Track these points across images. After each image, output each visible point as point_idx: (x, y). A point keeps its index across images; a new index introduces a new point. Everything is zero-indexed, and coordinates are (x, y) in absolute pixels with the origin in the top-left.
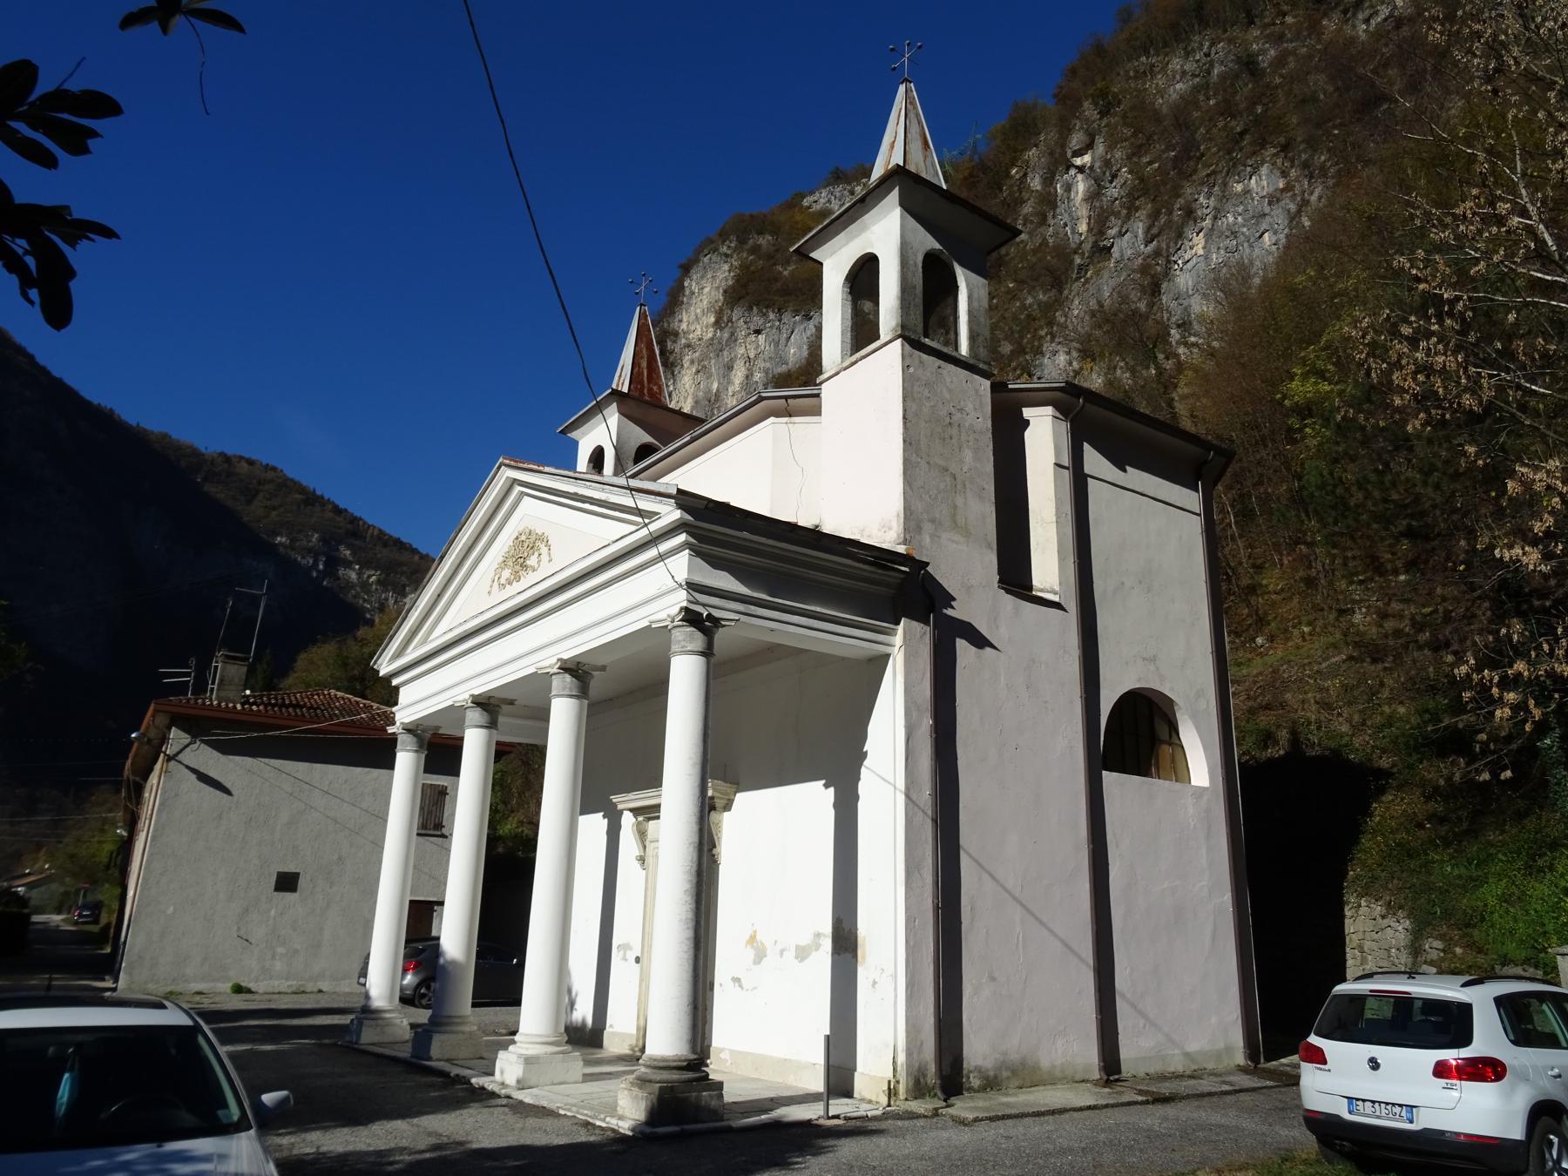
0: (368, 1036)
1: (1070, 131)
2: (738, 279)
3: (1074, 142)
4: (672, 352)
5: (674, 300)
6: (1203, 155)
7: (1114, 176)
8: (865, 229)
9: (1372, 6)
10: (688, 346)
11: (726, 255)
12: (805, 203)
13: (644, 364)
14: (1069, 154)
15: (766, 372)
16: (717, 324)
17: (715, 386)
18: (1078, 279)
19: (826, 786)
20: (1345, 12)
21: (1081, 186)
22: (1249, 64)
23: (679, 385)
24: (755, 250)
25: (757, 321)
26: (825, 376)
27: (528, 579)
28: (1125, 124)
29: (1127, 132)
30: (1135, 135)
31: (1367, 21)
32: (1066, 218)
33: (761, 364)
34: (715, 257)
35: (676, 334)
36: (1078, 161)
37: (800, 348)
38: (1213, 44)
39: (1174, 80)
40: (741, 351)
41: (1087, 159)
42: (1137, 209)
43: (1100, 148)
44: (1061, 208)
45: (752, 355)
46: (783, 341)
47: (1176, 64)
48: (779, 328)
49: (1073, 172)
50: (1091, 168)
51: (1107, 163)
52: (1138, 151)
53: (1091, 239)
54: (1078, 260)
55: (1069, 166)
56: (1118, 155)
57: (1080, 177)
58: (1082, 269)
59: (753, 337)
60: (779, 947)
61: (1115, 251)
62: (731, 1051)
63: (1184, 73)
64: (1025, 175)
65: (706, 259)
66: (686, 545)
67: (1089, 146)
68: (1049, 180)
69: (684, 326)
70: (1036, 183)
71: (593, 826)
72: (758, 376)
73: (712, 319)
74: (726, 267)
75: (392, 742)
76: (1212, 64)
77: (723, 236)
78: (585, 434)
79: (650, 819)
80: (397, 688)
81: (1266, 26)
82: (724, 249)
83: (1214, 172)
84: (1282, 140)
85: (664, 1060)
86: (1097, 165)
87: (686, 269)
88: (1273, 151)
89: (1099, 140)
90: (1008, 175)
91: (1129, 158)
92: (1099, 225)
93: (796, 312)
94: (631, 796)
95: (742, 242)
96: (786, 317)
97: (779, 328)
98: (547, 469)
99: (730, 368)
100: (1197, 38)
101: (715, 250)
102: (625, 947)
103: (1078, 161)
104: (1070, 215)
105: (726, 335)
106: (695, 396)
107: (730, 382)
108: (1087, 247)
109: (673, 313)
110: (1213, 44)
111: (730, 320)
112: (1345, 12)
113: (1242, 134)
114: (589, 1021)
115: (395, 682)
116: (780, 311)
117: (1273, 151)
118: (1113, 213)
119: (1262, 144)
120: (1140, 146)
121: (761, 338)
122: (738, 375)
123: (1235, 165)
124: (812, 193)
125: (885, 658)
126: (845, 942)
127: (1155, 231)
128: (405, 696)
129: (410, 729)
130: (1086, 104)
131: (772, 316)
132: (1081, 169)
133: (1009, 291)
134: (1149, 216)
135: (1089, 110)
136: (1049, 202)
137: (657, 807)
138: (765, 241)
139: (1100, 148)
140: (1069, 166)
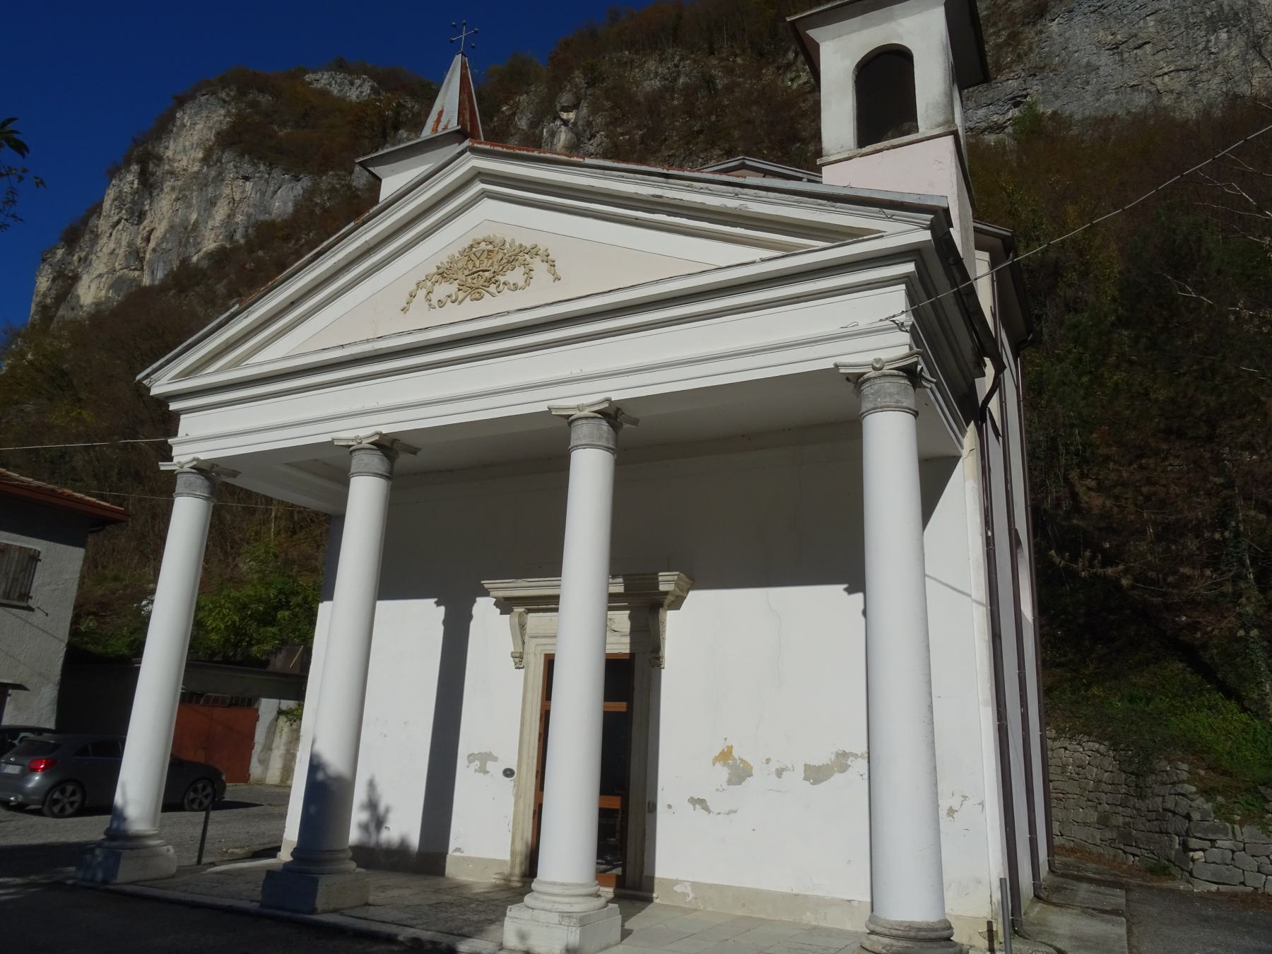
0: (126, 873)
1: (561, 89)
2: (233, 126)
3: (564, 99)
4: (153, 174)
5: (164, 127)
6: (666, 140)
7: (593, 136)
8: (890, 19)
9: (797, 71)
10: (172, 173)
11: (225, 102)
12: (308, 78)
13: (467, 117)
14: (558, 108)
15: (249, 216)
16: (205, 160)
17: (194, 217)
19: (438, 604)
20: (778, 68)
22: (709, 82)
23: (155, 206)
24: (254, 104)
25: (247, 168)
26: (824, 160)
27: (489, 304)
28: (607, 99)
29: (608, 104)
30: (612, 108)
31: (792, 80)
33: (244, 207)
34: (212, 99)
35: (160, 159)
36: (564, 116)
37: (285, 203)
38: (682, 59)
39: (649, 77)
40: (227, 191)
41: (571, 116)
43: (584, 111)
45: (237, 198)
46: (269, 193)
47: (651, 65)
48: (267, 181)
49: (558, 122)
50: (575, 124)
51: (589, 124)
52: (614, 122)
55: (556, 117)
56: (599, 120)
59: (240, 182)
60: (774, 766)
62: (695, 885)
63: (656, 74)
64: (514, 114)
65: (203, 99)
66: (905, 279)
67: (575, 106)
68: (536, 123)
69: (169, 153)
70: (523, 124)
71: (422, 618)
72: (239, 218)
73: (200, 155)
74: (222, 112)
75: (167, 487)
76: (679, 75)
77: (224, 83)
78: (394, 172)
79: (530, 611)
80: (176, 416)
81: (722, 59)
82: (223, 95)
83: (673, 155)
84: (727, 146)
85: (911, 926)
86: (580, 123)
87: (181, 102)
88: (720, 152)
89: (584, 104)
90: (499, 110)
91: (607, 125)
93: (287, 171)
95: (242, 93)
96: (276, 173)
97: (267, 181)
98: (588, 161)
99: (212, 203)
100: (670, 51)
101: (214, 93)
102: (483, 759)
103: (564, 116)
105: (213, 173)
106: (171, 220)
107: (210, 216)
109: (159, 138)
110: (682, 59)
111: (219, 160)
112: (778, 68)
113: (700, 132)
114: (415, 840)
115: (173, 406)
116: (271, 166)
117: (720, 152)
119: (713, 144)
120: (616, 119)
121: (249, 185)
122: (220, 212)
123: (691, 154)
124: (314, 72)
125: (955, 459)
128: (187, 426)
129: (205, 470)
130: (577, 72)
131: (262, 168)
132: (565, 123)
135: (579, 78)
137: (555, 599)
138: (265, 100)
139: (584, 111)
140: (556, 117)
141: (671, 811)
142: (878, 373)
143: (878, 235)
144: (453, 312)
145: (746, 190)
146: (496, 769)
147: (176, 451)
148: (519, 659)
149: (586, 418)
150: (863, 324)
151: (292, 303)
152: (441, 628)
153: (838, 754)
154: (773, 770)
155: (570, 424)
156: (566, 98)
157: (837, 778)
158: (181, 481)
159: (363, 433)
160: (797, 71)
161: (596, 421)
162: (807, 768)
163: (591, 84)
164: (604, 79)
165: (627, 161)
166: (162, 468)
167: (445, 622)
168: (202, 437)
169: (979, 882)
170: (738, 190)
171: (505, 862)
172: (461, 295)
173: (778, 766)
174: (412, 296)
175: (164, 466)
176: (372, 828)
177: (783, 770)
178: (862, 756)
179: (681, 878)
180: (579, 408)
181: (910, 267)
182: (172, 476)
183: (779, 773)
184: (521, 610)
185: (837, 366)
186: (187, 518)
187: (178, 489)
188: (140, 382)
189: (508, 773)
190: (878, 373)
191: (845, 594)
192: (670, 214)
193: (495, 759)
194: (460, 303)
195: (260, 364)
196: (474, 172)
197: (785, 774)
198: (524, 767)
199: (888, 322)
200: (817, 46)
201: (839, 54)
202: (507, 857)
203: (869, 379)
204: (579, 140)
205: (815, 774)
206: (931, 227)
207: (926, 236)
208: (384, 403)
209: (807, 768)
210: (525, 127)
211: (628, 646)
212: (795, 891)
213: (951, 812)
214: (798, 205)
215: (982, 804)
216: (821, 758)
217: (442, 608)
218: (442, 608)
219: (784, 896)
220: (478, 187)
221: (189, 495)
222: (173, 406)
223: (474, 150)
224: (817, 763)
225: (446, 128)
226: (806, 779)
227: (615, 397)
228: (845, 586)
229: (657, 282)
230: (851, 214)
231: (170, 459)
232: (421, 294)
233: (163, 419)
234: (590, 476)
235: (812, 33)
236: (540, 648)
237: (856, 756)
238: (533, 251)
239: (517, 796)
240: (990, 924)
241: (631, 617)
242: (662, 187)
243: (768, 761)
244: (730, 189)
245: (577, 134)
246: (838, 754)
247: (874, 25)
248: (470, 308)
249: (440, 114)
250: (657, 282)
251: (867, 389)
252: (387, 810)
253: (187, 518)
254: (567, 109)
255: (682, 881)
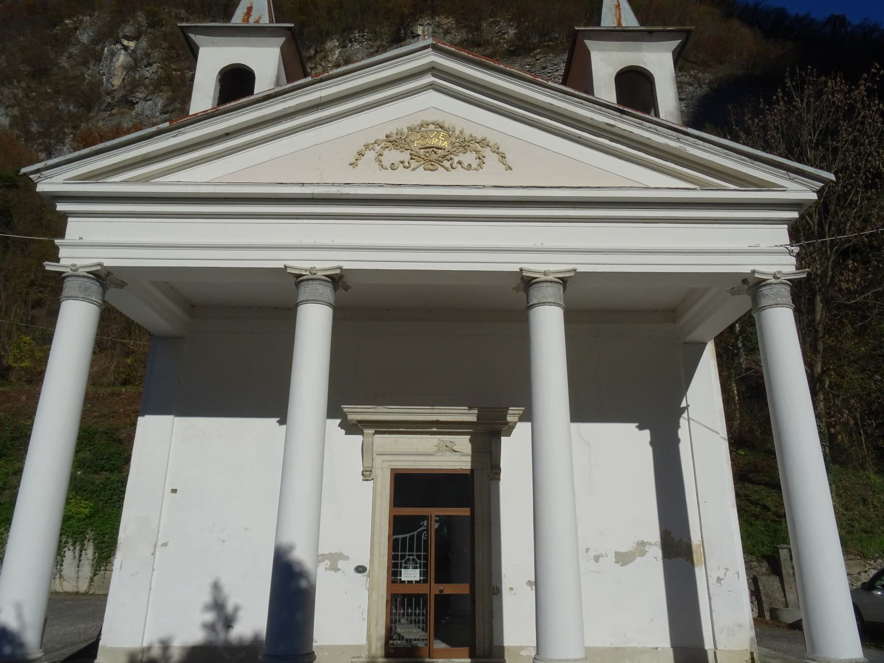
1: (125, 22)
7: (150, 65)
8: (638, 50)
9: (316, 64)
18: (105, 110)
19: (640, 428)
21: (122, 58)
27: (440, 176)
28: (165, 41)
32: (105, 70)
36: (125, 42)
41: (132, 44)
42: (161, 91)
43: (144, 43)
44: (104, 63)
49: (119, 46)
50: (134, 51)
51: (148, 55)
53: (123, 92)
54: (109, 99)
56: (156, 54)
57: (123, 52)
58: (110, 106)
60: (592, 553)
61: (138, 108)
64: (76, 29)
67: (136, 38)
79: (377, 433)
80: (64, 217)
86: (139, 52)
90: (62, 22)
91: (163, 60)
92: (132, 86)
94: (380, 409)
103: (125, 42)
104: (109, 70)
108: (118, 95)
115: (61, 207)
118: (143, 85)
120: (172, 57)
126: (677, 548)
127: (170, 108)
128: (74, 227)
129: (104, 278)
132: (126, 48)
133: (46, 93)
134: (168, 99)
135: (141, 17)
136: (93, 55)
139: (144, 43)
140: (117, 41)
141: (513, 592)
142: (778, 281)
143: (783, 189)
144: (402, 176)
145: (687, 137)
146: (347, 567)
147: (62, 253)
148: (367, 474)
149: (551, 282)
150: (763, 246)
151: (227, 134)
152: (649, 450)
153: (638, 544)
154: (592, 557)
155: (297, 285)
156: (128, 29)
157: (639, 559)
158: (69, 286)
159: (319, 265)
160: (316, 64)
161: (557, 286)
162: (617, 554)
163: (152, 25)
164: (162, 26)
165: (580, 90)
166: (48, 268)
167: (652, 443)
168: (89, 243)
169: (740, 626)
170: (681, 135)
171: (362, 646)
172: (414, 164)
173: (595, 554)
174: (361, 154)
175: (50, 266)
176: (220, 627)
177: (599, 556)
178: (655, 544)
179: (523, 645)
180: (545, 273)
181: (795, 215)
182: (59, 278)
183: (597, 559)
184: (372, 431)
185: (754, 272)
186: (75, 325)
187: (66, 292)
188: (26, 175)
189: (360, 569)
190: (778, 281)
191: (637, 430)
192: (612, 140)
193: (347, 558)
194: (414, 169)
195: (179, 183)
196: (430, 66)
197: (601, 559)
198: (376, 563)
199: (782, 248)
200: (198, 48)
201: (213, 58)
202: (363, 641)
203: (770, 284)
204: (136, 64)
205: (623, 559)
206: (819, 192)
207: (814, 196)
208: (339, 242)
209: (617, 554)
210: (86, 42)
211: (470, 464)
212: (614, 646)
213: (719, 580)
214: (726, 157)
215: (738, 573)
216: (627, 546)
217: (647, 433)
218: (647, 433)
219: (608, 650)
220: (429, 79)
221: (84, 299)
222: (61, 207)
223: (435, 48)
224: (624, 550)
225: (257, 22)
226: (617, 562)
227: (107, 263)
228: (278, 419)
229: (619, 188)
230: (764, 171)
231: (57, 260)
232: (370, 155)
233: (48, 221)
234: (314, 325)
235: (588, 43)
236: (386, 464)
237: (651, 544)
238: (483, 143)
239: (370, 590)
240: (752, 654)
241: (471, 441)
242: (615, 119)
243: (587, 550)
244: (675, 133)
245: (136, 60)
246: (638, 544)
247: (628, 51)
248: (421, 175)
249: (250, 9)
250: (619, 188)
251: (765, 290)
252: (236, 609)
253: (75, 325)
254: (128, 38)
255: (527, 647)
